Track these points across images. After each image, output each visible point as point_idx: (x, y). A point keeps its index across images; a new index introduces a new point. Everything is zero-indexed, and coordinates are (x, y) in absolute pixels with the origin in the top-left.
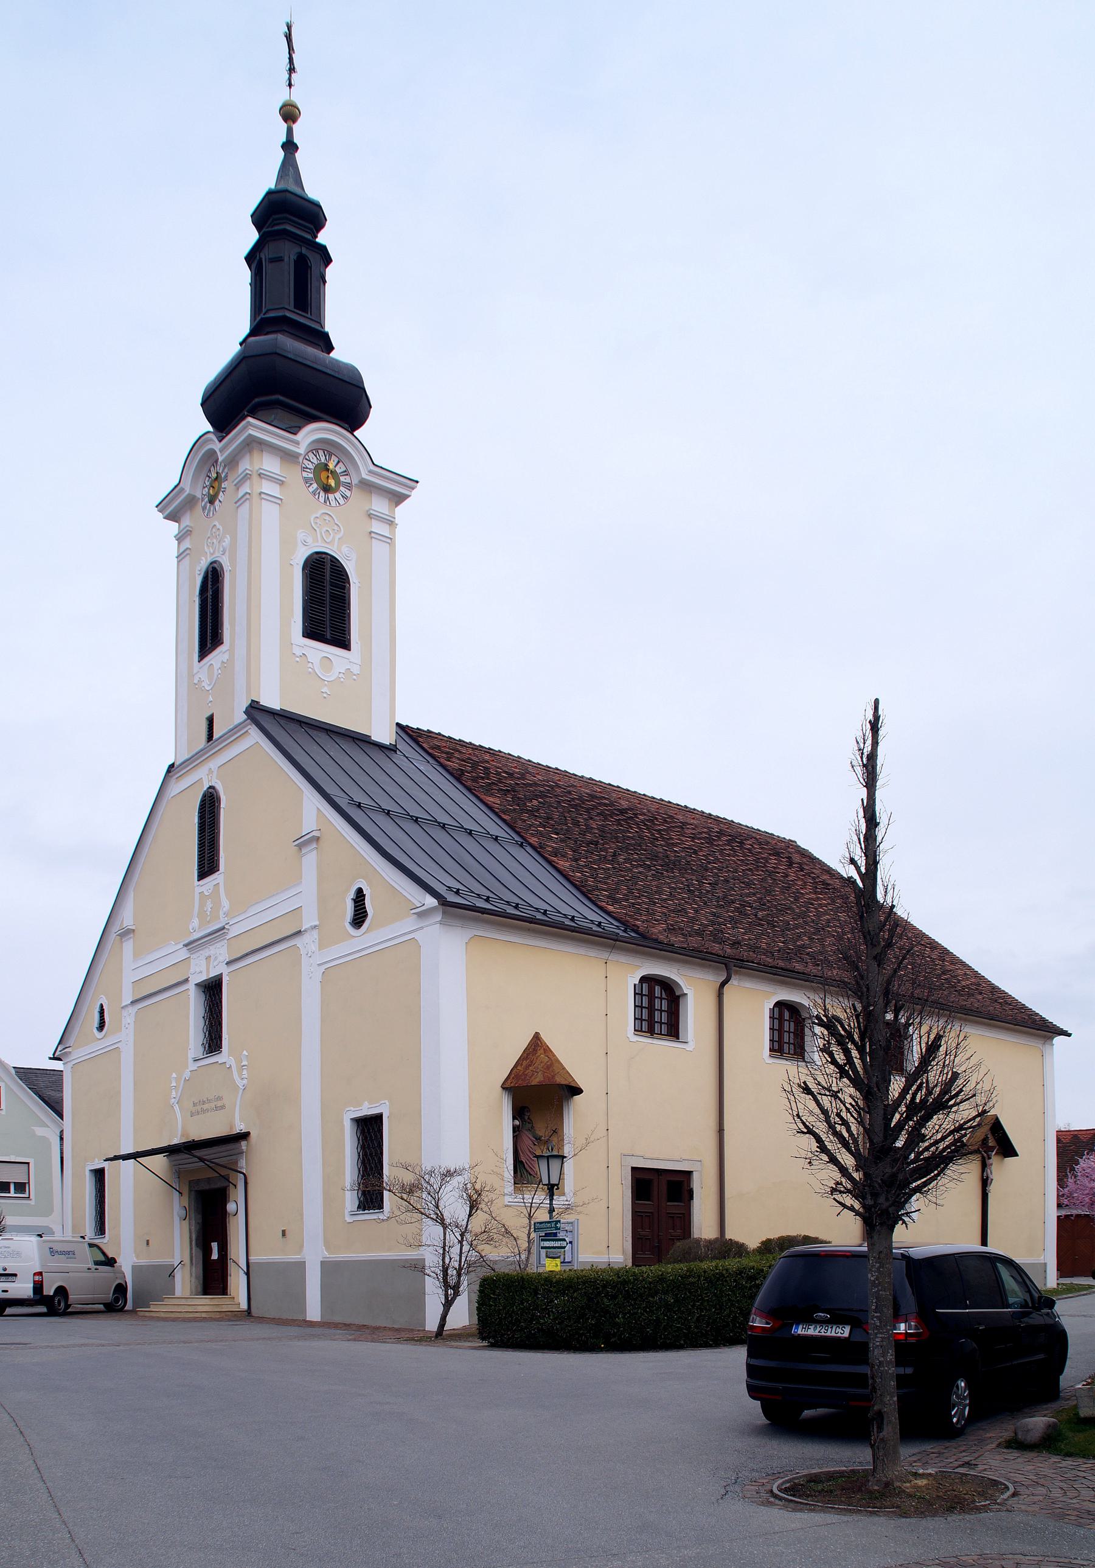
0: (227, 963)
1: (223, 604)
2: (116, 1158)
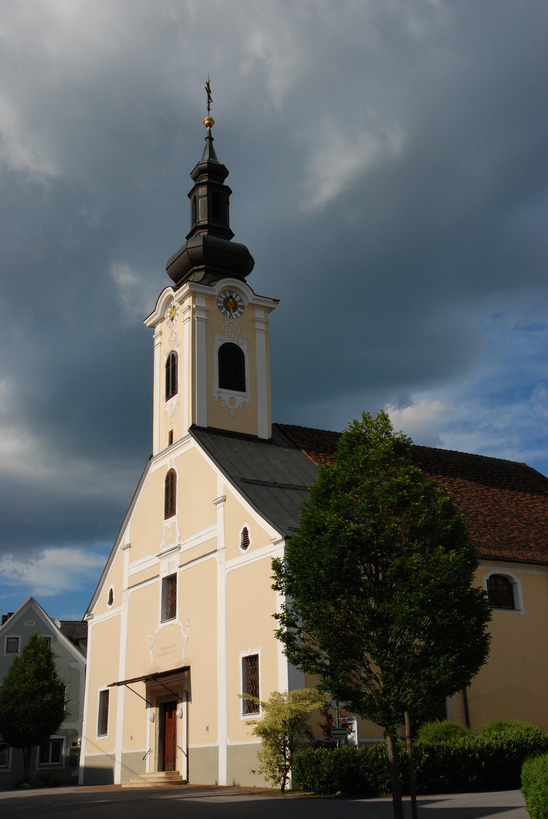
0: (180, 567)
2: (114, 684)
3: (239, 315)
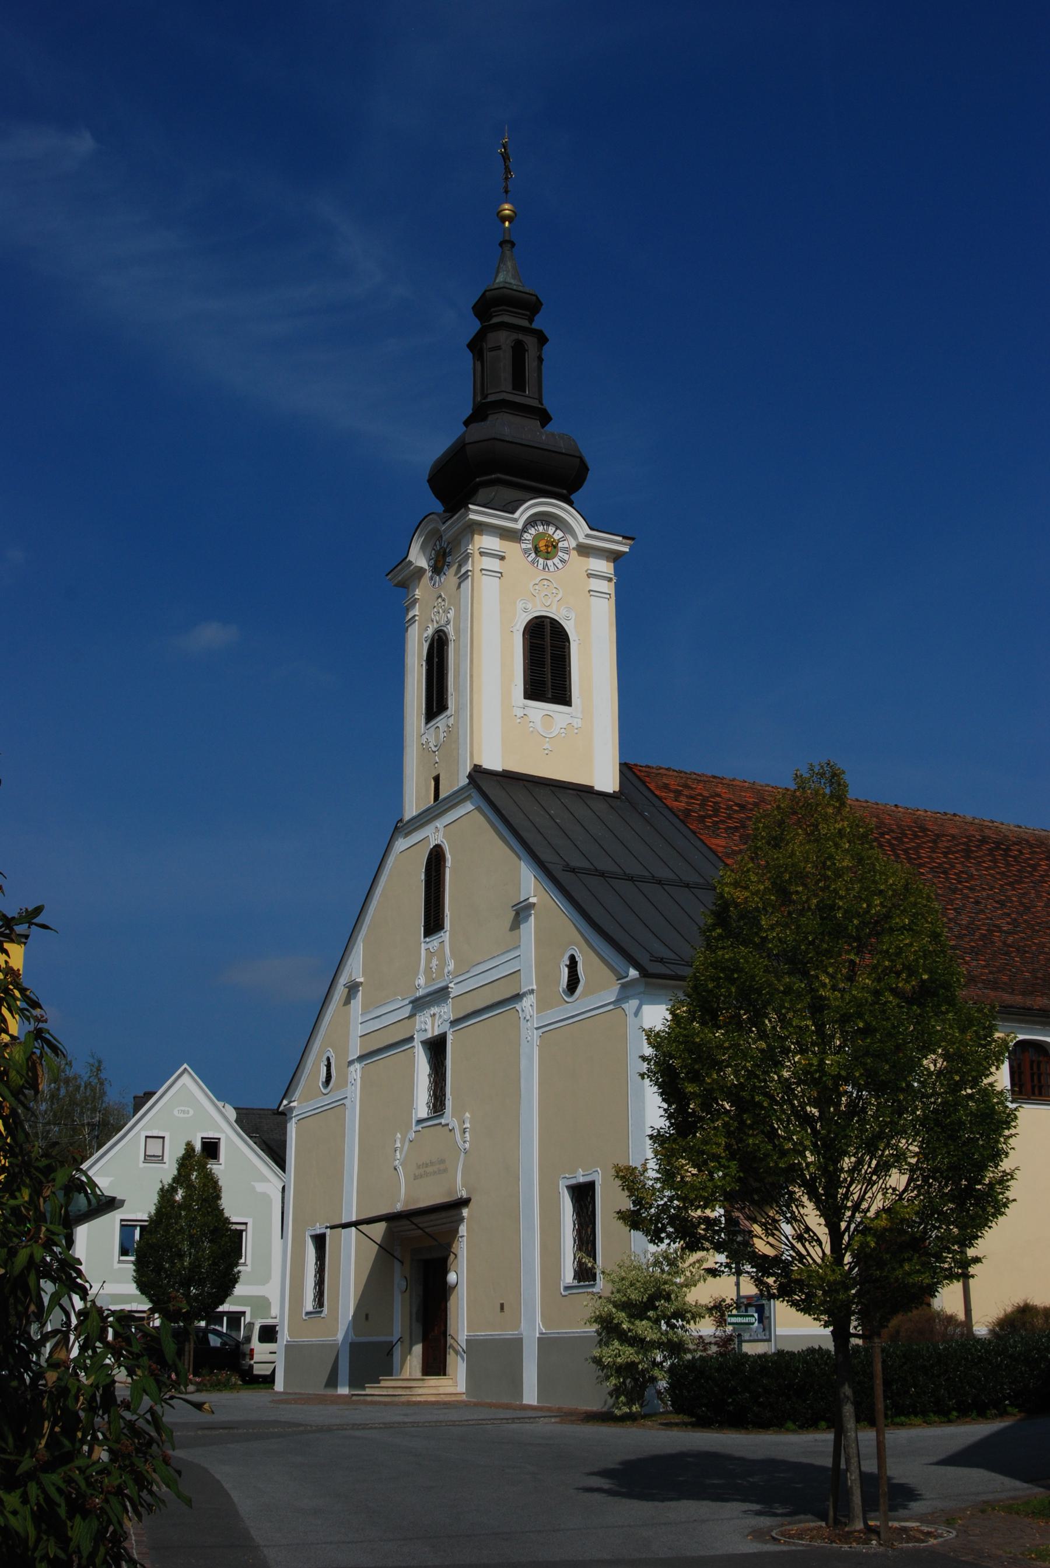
1: (447, 670)
3: (560, 566)
